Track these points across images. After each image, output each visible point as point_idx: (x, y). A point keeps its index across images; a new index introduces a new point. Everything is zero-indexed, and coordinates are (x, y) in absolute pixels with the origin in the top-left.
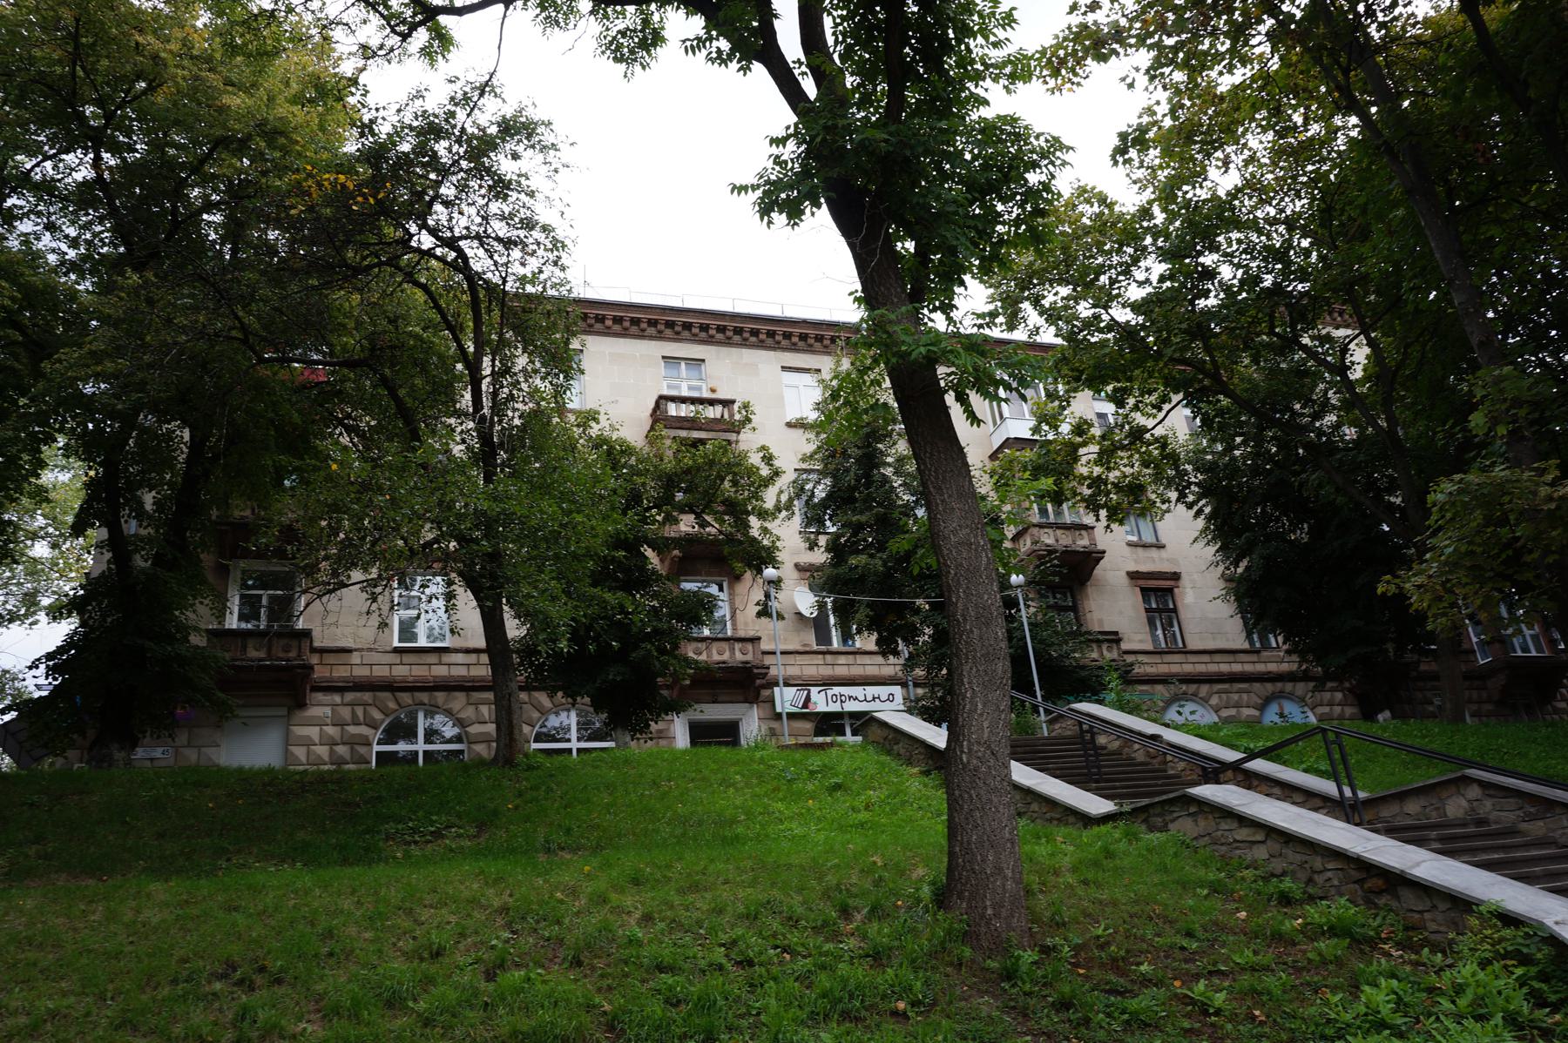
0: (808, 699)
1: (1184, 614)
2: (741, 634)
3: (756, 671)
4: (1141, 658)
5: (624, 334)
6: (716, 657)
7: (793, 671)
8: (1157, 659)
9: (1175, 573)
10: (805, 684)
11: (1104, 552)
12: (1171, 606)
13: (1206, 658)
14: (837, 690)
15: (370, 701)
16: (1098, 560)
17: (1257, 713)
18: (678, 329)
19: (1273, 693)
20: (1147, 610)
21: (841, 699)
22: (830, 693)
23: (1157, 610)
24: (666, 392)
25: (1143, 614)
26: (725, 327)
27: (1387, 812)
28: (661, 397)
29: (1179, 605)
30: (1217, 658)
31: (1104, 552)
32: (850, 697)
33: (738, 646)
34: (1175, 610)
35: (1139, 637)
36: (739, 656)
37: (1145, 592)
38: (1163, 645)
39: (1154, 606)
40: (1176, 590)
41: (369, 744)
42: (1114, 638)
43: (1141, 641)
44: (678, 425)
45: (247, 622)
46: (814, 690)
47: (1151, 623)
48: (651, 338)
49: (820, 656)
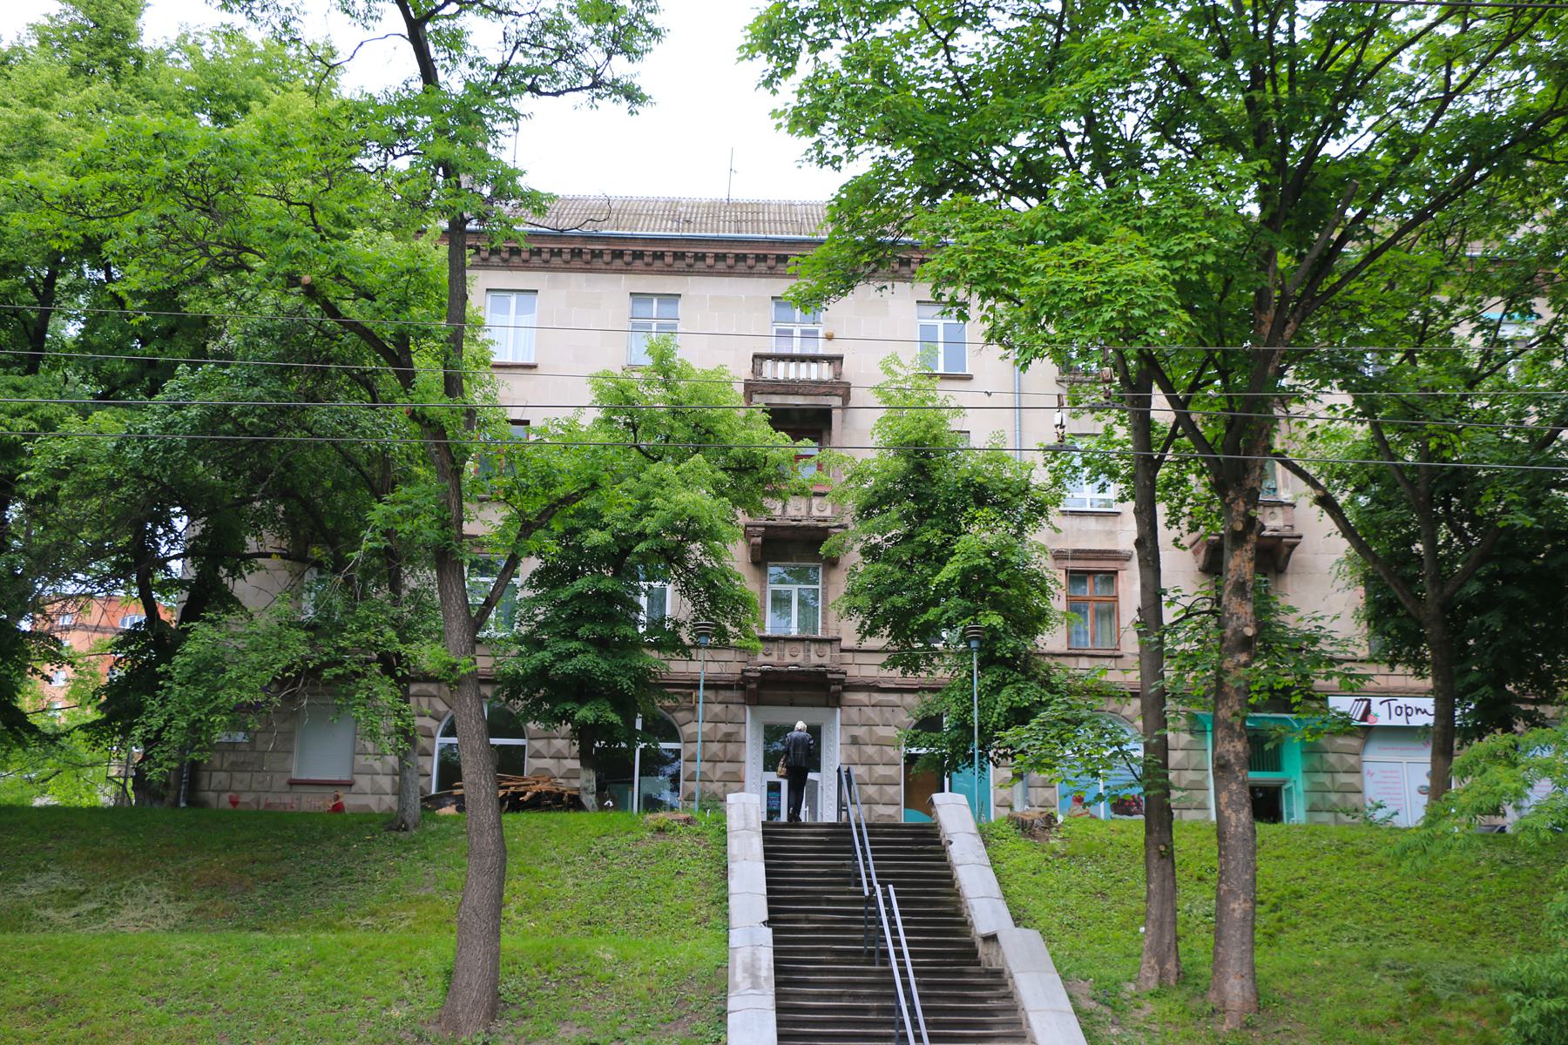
0: (1368, 711)
3: (829, 676)
5: (730, 272)
6: (788, 659)
11: (1300, 537)
14: (1402, 701)
15: (435, 693)
16: (1293, 547)
18: (505, 255)
21: (1407, 711)
22: (1394, 704)
24: (771, 347)
28: (756, 356)
31: (1300, 537)
32: (1418, 710)
33: (813, 647)
36: (814, 659)
41: (432, 737)
44: (771, 390)
45: (927, 622)
46: (1375, 701)
48: (761, 275)
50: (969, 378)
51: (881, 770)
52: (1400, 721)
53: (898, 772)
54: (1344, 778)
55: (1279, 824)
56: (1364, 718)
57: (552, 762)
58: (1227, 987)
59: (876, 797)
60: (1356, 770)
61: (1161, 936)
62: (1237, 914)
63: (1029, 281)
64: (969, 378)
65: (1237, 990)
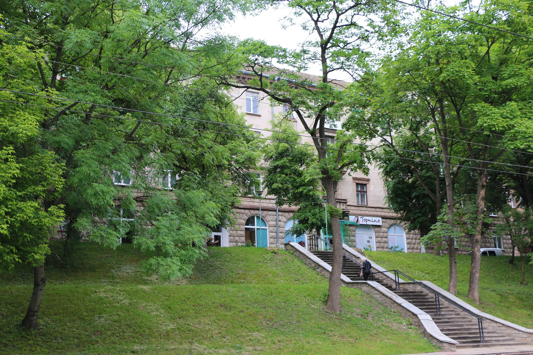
0: (358, 220)
1: (369, 193)
2: (369, 205)
4: (352, 208)
7: (355, 212)
8: (357, 208)
9: (368, 179)
10: (357, 215)
12: (365, 190)
13: (373, 209)
14: (365, 218)
17: (386, 230)
19: (393, 224)
20: (357, 191)
21: (366, 220)
23: (361, 191)
25: (356, 192)
26: (245, 78)
27: (377, 272)
29: (367, 190)
30: (377, 210)
34: (366, 192)
35: (353, 200)
37: (357, 184)
38: (360, 204)
39: (359, 190)
40: (367, 185)
42: (344, 202)
43: (353, 202)
47: (358, 195)
49: (249, 199)
50: (260, 116)
51: (239, 232)
52: (364, 223)
53: (243, 233)
54: (352, 238)
55: (218, 247)
56: (357, 222)
57: (380, 239)
58: (475, 294)
59: (238, 240)
60: (386, 237)
61: (118, 283)
62: (477, 277)
63: (32, 45)
64: (260, 116)
65: (477, 295)
